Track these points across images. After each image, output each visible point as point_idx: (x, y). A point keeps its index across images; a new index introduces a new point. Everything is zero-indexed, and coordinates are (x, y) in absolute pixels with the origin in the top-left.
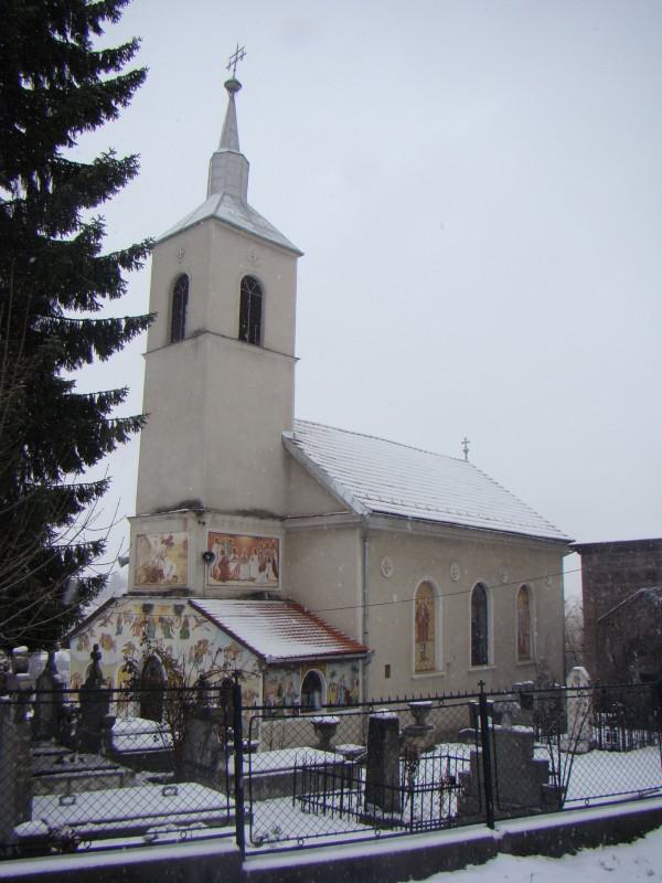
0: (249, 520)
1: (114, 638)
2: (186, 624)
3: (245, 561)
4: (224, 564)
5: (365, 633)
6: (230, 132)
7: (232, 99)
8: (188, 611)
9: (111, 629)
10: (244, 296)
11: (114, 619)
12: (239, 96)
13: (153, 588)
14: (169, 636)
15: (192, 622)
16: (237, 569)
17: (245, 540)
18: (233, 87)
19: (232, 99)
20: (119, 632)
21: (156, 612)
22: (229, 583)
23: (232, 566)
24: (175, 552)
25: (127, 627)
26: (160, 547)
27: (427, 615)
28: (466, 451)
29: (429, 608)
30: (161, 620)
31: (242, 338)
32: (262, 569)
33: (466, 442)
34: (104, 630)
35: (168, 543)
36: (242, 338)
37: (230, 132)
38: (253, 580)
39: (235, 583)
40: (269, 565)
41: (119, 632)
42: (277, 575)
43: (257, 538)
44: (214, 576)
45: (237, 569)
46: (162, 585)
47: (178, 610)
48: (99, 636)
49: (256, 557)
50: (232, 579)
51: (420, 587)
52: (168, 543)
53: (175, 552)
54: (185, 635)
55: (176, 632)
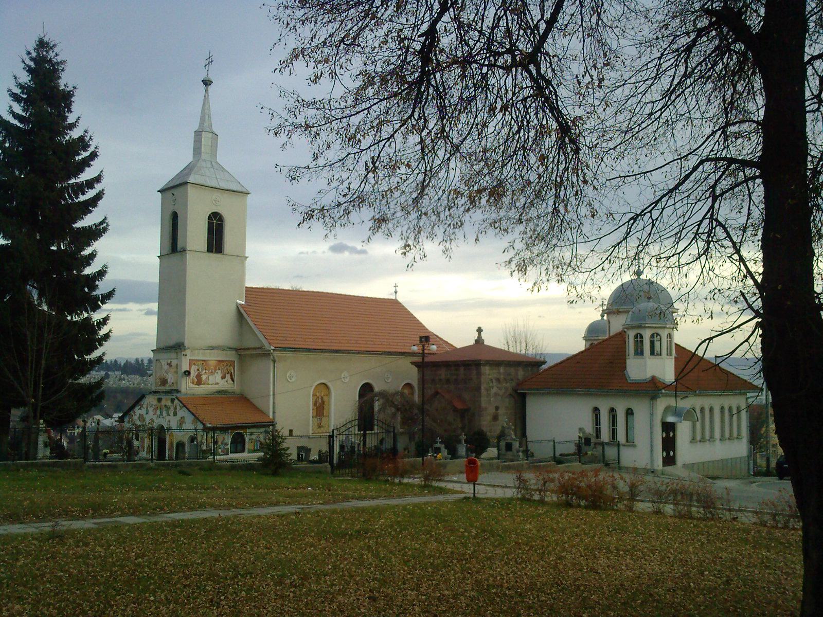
0: (215, 352)
1: (145, 416)
2: (176, 408)
3: (212, 373)
4: (199, 376)
5: (274, 412)
6: (205, 116)
7: (206, 91)
8: (176, 401)
9: (143, 411)
10: (210, 225)
11: (145, 406)
12: (210, 88)
13: (162, 388)
14: (169, 415)
15: (178, 407)
16: (207, 378)
17: (212, 363)
18: (207, 83)
19: (206, 91)
20: (147, 413)
21: (163, 403)
22: (203, 386)
23: (204, 377)
24: (173, 370)
25: (151, 410)
26: (166, 367)
27: (323, 402)
28: (396, 292)
29: (325, 399)
30: (165, 406)
31: (210, 249)
32: (223, 377)
33: (396, 286)
34: (140, 412)
35: (170, 364)
36: (210, 249)
37: (205, 116)
38: (218, 384)
39: (205, 386)
40: (228, 376)
41: (147, 413)
42: (233, 380)
43: (219, 361)
44: (193, 383)
45: (207, 378)
46: (167, 388)
47: (172, 401)
48: (138, 415)
49: (219, 372)
50: (204, 384)
51: (316, 386)
52: (170, 364)
53: (173, 370)
54: (175, 414)
55: (172, 412)
